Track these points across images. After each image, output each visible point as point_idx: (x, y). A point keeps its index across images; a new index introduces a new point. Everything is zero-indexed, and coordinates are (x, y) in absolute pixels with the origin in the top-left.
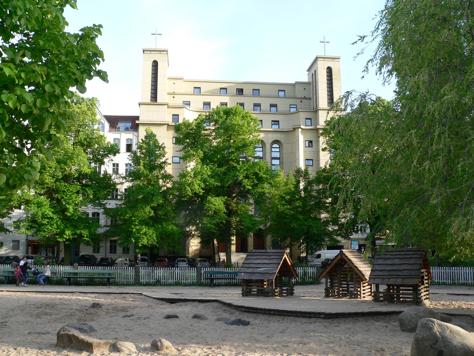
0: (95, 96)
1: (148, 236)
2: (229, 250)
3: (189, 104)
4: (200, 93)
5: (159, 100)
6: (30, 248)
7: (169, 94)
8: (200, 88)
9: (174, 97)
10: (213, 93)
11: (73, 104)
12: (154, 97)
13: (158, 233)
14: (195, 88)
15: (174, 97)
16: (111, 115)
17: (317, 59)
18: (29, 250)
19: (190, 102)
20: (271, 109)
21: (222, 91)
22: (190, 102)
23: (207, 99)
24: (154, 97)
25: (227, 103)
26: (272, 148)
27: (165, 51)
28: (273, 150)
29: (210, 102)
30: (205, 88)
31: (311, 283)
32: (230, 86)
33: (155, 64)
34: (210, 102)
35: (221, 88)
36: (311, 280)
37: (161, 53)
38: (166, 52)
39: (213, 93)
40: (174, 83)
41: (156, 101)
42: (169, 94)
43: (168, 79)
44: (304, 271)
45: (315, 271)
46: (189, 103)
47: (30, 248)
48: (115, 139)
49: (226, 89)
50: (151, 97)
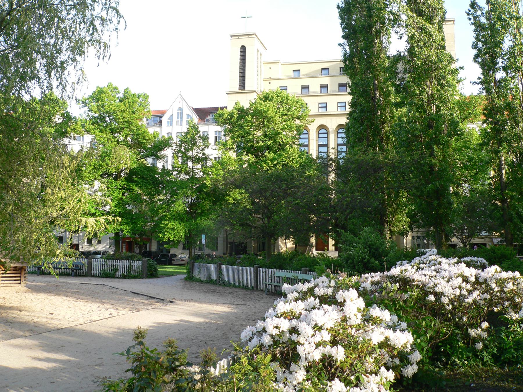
0: (146, 92)
1: (176, 231)
2: (272, 247)
3: (287, 89)
4: (299, 77)
5: (247, 88)
6: (124, 244)
7: (265, 80)
8: (299, 70)
9: (270, 83)
10: (313, 75)
11: (112, 102)
12: (242, 85)
13: (187, 229)
14: (294, 71)
15: (270, 83)
16: (205, 107)
17: (255, 34)
18: (124, 247)
19: (287, 87)
20: (303, 91)
21: (324, 71)
22: (287, 87)
23: (305, 82)
24: (242, 85)
25: (327, 85)
26: (338, 133)
27: (452, 20)
28: (320, 136)
29: (327, 85)
30: (305, 70)
31: (135, 277)
32: (332, 66)
33: (243, 49)
34: (309, 85)
35: (322, 69)
36: (137, 274)
37: (249, 37)
38: (452, 22)
39: (313, 75)
40: (270, 68)
41: (244, 89)
42: (265, 80)
43: (263, 63)
44: (130, 264)
45: (141, 264)
46: (286, 88)
47: (124, 244)
48: (168, 133)
49: (328, 69)
50: (239, 85)
